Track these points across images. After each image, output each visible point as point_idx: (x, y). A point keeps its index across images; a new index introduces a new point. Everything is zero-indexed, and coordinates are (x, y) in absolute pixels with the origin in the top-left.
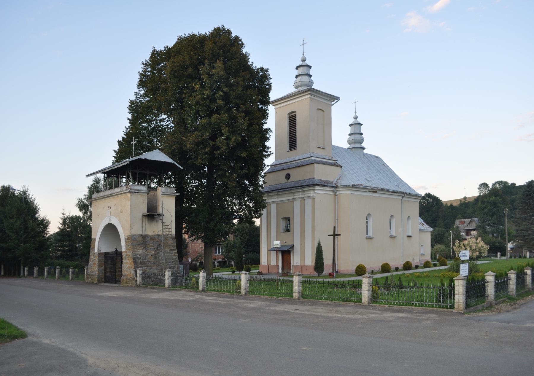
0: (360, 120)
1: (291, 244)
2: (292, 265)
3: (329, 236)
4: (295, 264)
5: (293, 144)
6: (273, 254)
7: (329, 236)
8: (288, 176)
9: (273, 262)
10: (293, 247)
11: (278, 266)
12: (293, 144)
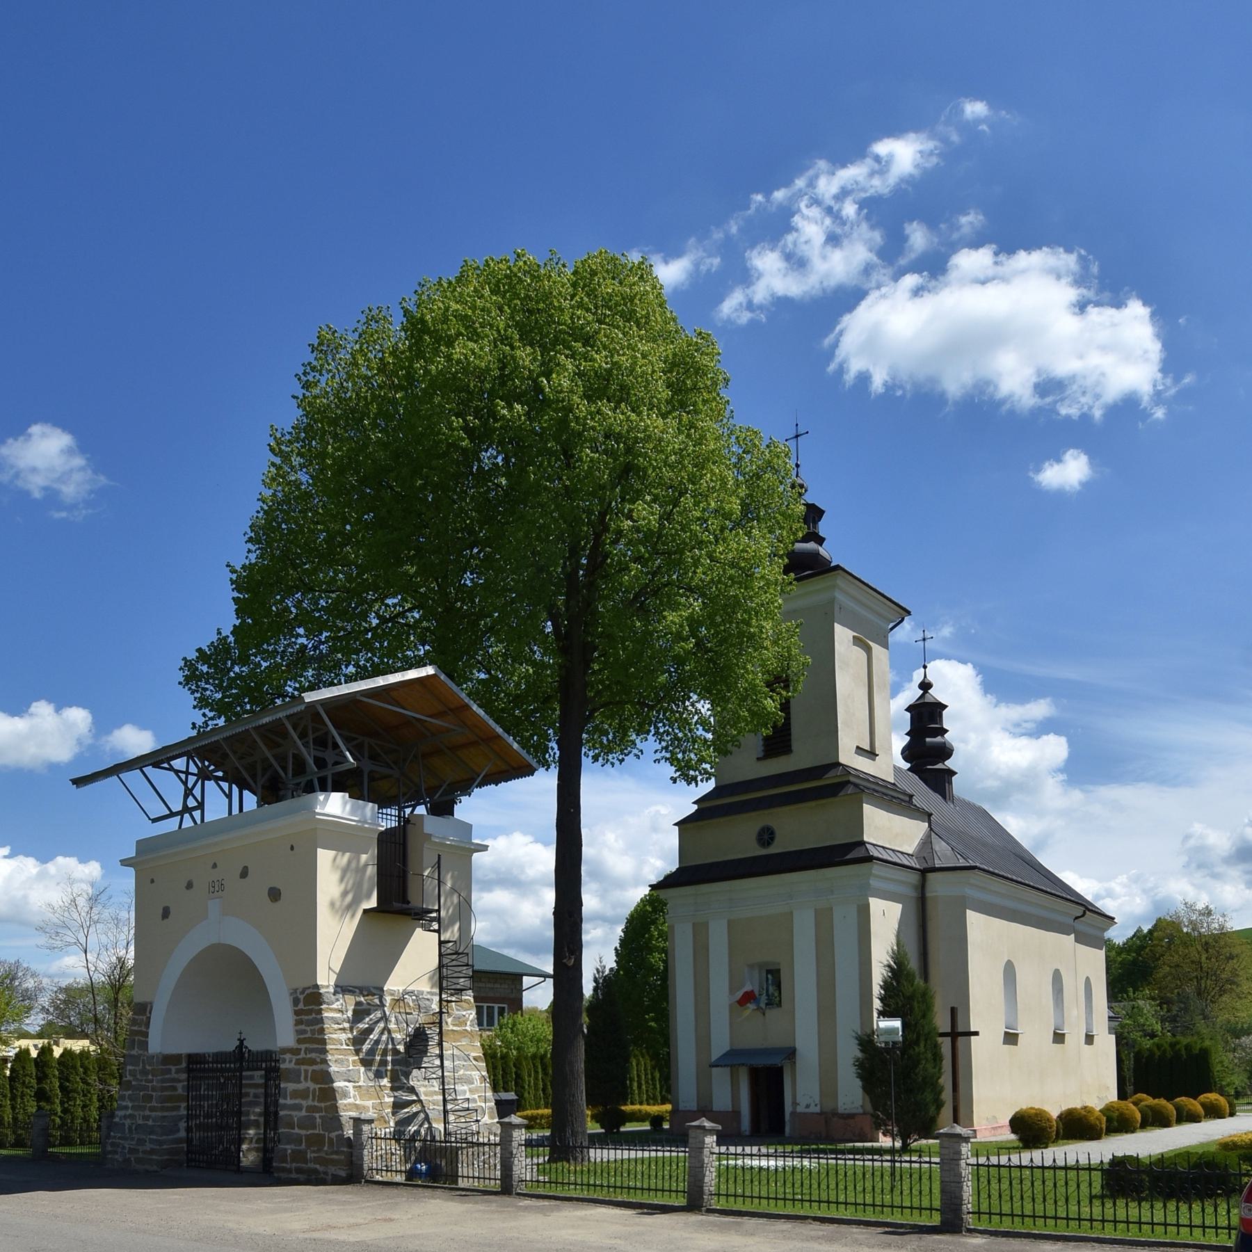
2: (788, 1109)
4: (800, 1109)
8: (767, 836)
10: (791, 1053)
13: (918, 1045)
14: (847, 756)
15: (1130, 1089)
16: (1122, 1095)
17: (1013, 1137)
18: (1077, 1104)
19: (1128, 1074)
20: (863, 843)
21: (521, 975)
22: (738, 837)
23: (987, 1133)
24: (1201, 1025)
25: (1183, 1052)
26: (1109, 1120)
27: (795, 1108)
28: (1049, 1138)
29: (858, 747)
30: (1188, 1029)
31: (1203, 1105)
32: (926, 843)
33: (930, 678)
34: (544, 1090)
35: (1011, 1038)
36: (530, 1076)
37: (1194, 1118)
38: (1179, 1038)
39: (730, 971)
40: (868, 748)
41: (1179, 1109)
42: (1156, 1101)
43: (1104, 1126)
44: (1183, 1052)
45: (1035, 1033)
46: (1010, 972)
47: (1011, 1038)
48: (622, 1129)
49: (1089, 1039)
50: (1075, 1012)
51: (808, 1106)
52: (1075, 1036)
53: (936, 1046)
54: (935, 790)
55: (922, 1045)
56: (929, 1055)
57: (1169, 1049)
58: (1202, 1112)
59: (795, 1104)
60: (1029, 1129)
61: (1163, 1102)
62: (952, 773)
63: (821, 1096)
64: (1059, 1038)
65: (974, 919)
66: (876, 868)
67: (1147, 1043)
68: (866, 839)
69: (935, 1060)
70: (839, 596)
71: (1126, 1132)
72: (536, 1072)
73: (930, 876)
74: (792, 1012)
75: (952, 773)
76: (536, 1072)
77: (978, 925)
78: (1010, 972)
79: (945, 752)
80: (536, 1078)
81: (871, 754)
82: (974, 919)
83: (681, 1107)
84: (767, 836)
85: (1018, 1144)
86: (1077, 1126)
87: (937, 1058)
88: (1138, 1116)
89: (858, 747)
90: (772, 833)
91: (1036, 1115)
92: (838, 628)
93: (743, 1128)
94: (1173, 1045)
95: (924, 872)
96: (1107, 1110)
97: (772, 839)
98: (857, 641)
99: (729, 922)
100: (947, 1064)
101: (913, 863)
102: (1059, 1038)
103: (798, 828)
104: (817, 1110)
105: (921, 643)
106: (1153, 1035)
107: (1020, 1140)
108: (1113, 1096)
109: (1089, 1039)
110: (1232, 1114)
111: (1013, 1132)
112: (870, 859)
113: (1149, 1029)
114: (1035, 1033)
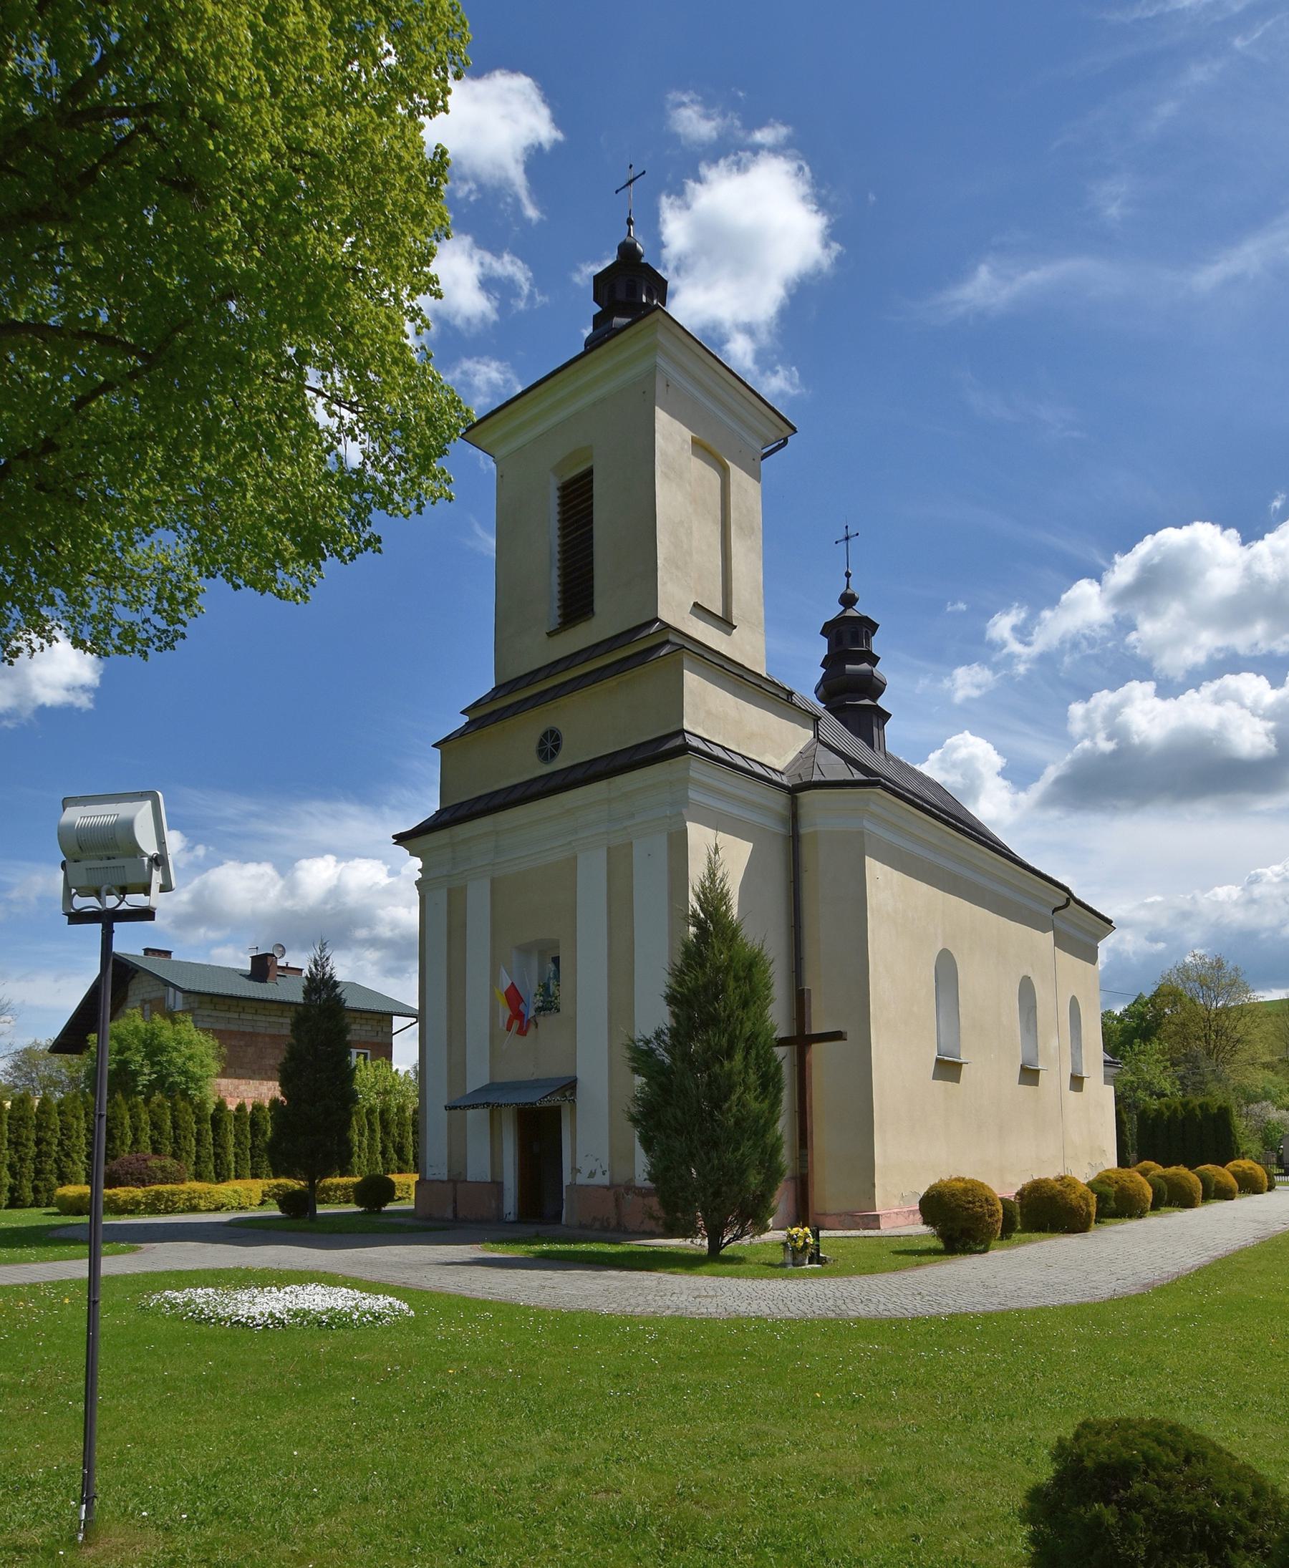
0: (859, 610)
1: (554, 1070)
2: (567, 1180)
3: (837, 1036)
4: (582, 1179)
5: (576, 600)
6: (477, 1119)
7: (837, 1036)
8: (550, 744)
9: (478, 1169)
10: (570, 1086)
11: (497, 1185)
12: (576, 600)
13: (730, 1057)
14: (673, 606)
15: (1133, 1156)
16: (1123, 1162)
17: (925, 1229)
18: (1050, 1173)
19: (1130, 1141)
20: (682, 732)
21: (391, 1015)
22: (515, 757)
23: (901, 1220)
24: (1212, 1086)
25: (1198, 1112)
26: (1102, 1198)
27: (574, 1178)
28: (991, 1234)
29: (696, 605)
30: (1199, 1087)
31: (1235, 1174)
32: (805, 756)
33: (854, 589)
34: (383, 1153)
35: (948, 1069)
36: (362, 1134)
37: (1224, 1194)
38: (1190, 1097)
39: (610, 998)
40: (717, 609)
41: (1205, 1180)
42: (1173, 1169)
43: (1093, 1210)
44: (1198, 1112)
45: (991, 1068)
46: (946, 971)
47: (948, 1069)
48: (387, 1208)
49: (1077, 1082)
50: (1054, 1042)
51: (592, 1175)
52: (1054, 1075)
53: (768, 1059)
54: (857, 735)
55: (738, 1057)
56: (753, 1078)
57: (1180, 1108)
58: (1235, 1185)
59: (575, 1171)
60: (958, 1221)
61: (1183, 1171)
62: (885, 716)
63: (611, 1156)
64: (1029, 1075)
65: (875, 870)
66: (697, 769)
67: (1154, 1104)
68: (686, 726)
69: (764, 1086)
70: (661, 362)
71: (1130, 1217)
72: (372, 1130)
73: (805, 797)
74: (573, 1019)
75: (885, 716)
76: (372, 1130)
77: (884, 885)
78: (946, 971)
79: (874, 687)
80: (372, 1138)
81: (725, 623)
82: (875, 870)
83: (429, 1176)
84: (550, 744)
85: (938, 1244)
86: (1048, 1211)
87: (769, 1083)
88: (1149, 1192)
89: (696, 605)
90: (558, 738)
91: (966, 1191)
92: (662, 418)
93: (506, 1210)
94: (1185, 1105)
95: (793, 791)
96: (1099, 1185)
97: (557, 747)
98: (700, 448)
99: (493, 881)
100: (787, 1097)
101: (784, 780)
102: (1029, 1075)
103: (591, 724)
104: (605, 1180)
105: (843, 544)
106: (1161, 1095)
107: (941, 1235)
108: (1111, 1161)
109: (1077, 1082)
110: (1270, 1188)
111: (925, 1223)
112: (685, 749)
113: (1157, 1089)
114: (991, 1068)
